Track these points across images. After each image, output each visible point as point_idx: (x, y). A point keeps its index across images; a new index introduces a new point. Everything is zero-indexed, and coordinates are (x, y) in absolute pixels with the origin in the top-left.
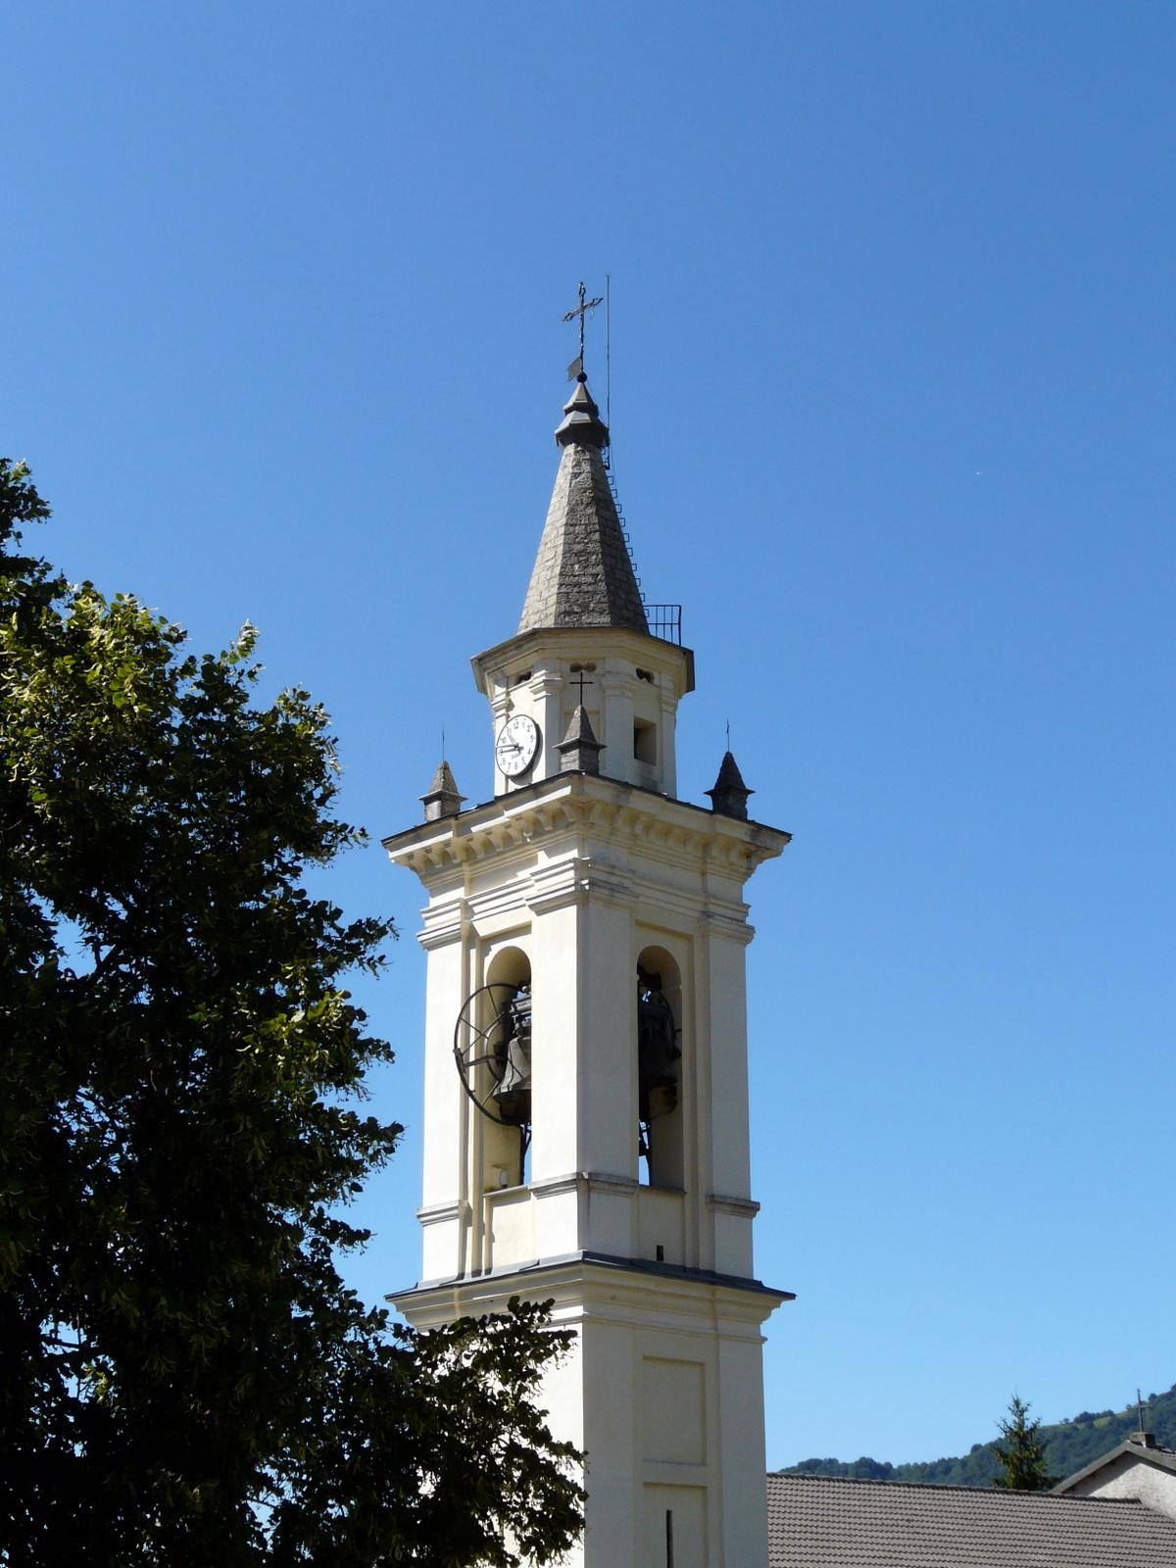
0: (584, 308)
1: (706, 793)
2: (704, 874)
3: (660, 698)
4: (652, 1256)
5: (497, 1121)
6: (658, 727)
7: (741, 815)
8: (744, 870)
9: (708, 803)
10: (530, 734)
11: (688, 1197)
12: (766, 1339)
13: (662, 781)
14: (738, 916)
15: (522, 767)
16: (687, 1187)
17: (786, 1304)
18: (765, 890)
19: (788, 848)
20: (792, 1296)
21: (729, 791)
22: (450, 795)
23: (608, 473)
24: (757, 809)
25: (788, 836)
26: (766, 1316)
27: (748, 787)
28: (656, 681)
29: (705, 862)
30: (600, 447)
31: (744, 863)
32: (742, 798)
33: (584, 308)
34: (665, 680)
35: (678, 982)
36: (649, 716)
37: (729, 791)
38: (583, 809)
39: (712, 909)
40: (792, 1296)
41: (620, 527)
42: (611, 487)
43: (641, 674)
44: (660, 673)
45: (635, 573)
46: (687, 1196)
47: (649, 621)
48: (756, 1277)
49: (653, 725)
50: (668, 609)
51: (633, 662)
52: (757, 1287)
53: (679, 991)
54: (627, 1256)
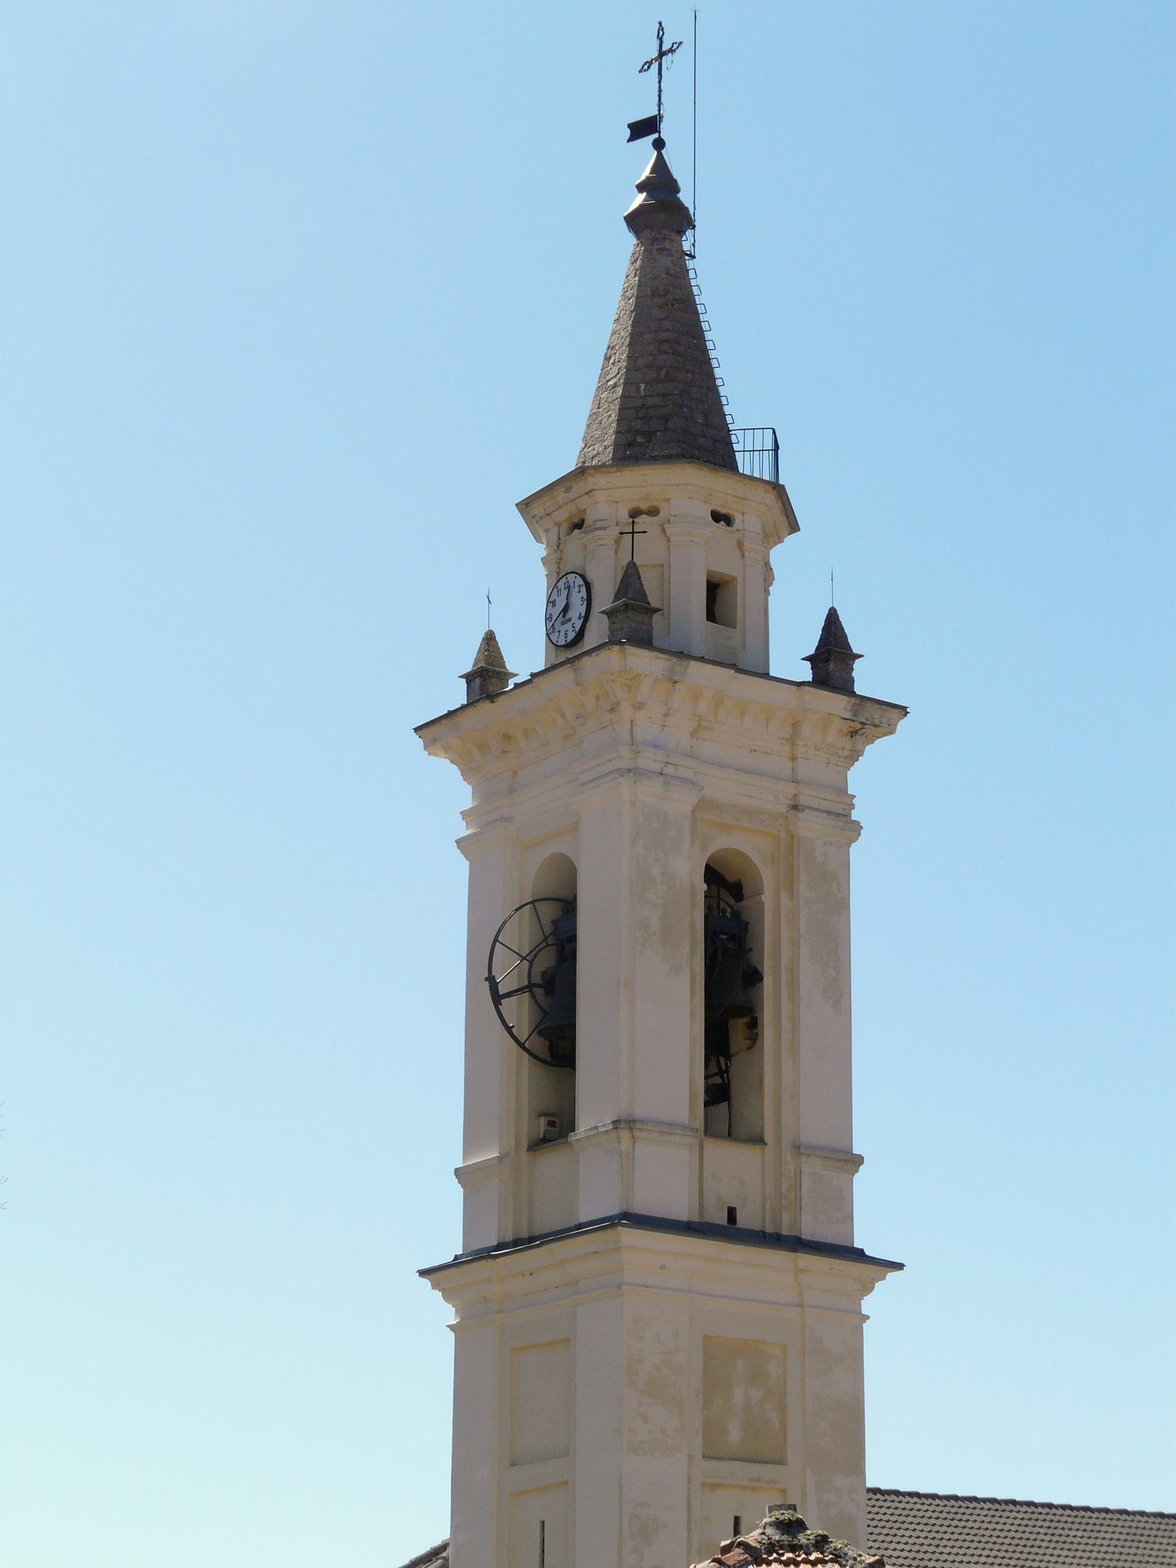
0: (662, 54)
1: (490, 639)
2: (794, 759)
3: (740, 544)
4: (722, 1218)
5: (543, 1061)
6: (739, 580)
7: (845, 687)
8: (846, 753)
9: (805, 673)
10: (581, 595)
11: (769, 1149)
12: (868, 1317)
13: (744, 647)
14: (836, 808)
15: (571, 636)
16: (769, 1137)
17: (892, 1276)
18: (876, 778)
19: (903, 725)
20: (899, 1266)
21: (833, 656)
22: (494, 671)
23: (690, 264)
24: (867, 679)
25: (903, 711)
26: (868, 1289)
27: (855, 651)
28: (738, 523)
29: (794, 744)
30: (681, 232)
31: (847, 743)
32: (847, 664)
33: (662, 54)
34: (748, 521)
35: (760, 892)
36: (726, 567)
37: (833, 656)
38: (629, 687)
39: (803, 800)
40: (899, 1266)
41: (702, 331)
42: (693, 282)
43: (717, 517)
44: (743, 514)
45: (721, 389)
46: (767, 1148)
47: (736, 447)
48: (857, 1245)
49: (733, 580)
50: (749, 433)
51: (705, 502)
52: (859, 1255)
53: (762, 904)
54: (685, 1218)
